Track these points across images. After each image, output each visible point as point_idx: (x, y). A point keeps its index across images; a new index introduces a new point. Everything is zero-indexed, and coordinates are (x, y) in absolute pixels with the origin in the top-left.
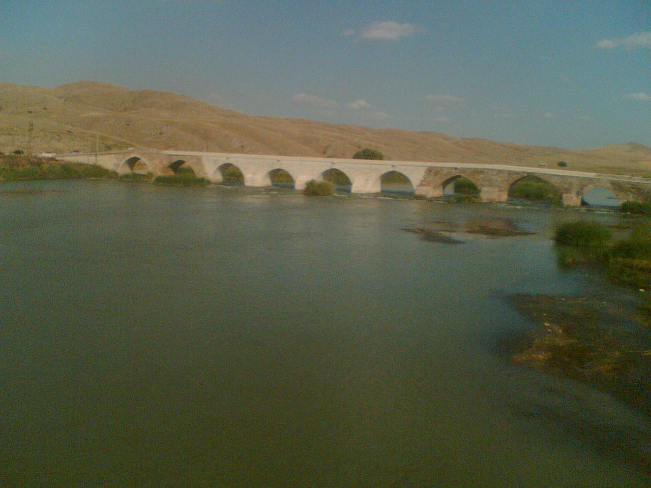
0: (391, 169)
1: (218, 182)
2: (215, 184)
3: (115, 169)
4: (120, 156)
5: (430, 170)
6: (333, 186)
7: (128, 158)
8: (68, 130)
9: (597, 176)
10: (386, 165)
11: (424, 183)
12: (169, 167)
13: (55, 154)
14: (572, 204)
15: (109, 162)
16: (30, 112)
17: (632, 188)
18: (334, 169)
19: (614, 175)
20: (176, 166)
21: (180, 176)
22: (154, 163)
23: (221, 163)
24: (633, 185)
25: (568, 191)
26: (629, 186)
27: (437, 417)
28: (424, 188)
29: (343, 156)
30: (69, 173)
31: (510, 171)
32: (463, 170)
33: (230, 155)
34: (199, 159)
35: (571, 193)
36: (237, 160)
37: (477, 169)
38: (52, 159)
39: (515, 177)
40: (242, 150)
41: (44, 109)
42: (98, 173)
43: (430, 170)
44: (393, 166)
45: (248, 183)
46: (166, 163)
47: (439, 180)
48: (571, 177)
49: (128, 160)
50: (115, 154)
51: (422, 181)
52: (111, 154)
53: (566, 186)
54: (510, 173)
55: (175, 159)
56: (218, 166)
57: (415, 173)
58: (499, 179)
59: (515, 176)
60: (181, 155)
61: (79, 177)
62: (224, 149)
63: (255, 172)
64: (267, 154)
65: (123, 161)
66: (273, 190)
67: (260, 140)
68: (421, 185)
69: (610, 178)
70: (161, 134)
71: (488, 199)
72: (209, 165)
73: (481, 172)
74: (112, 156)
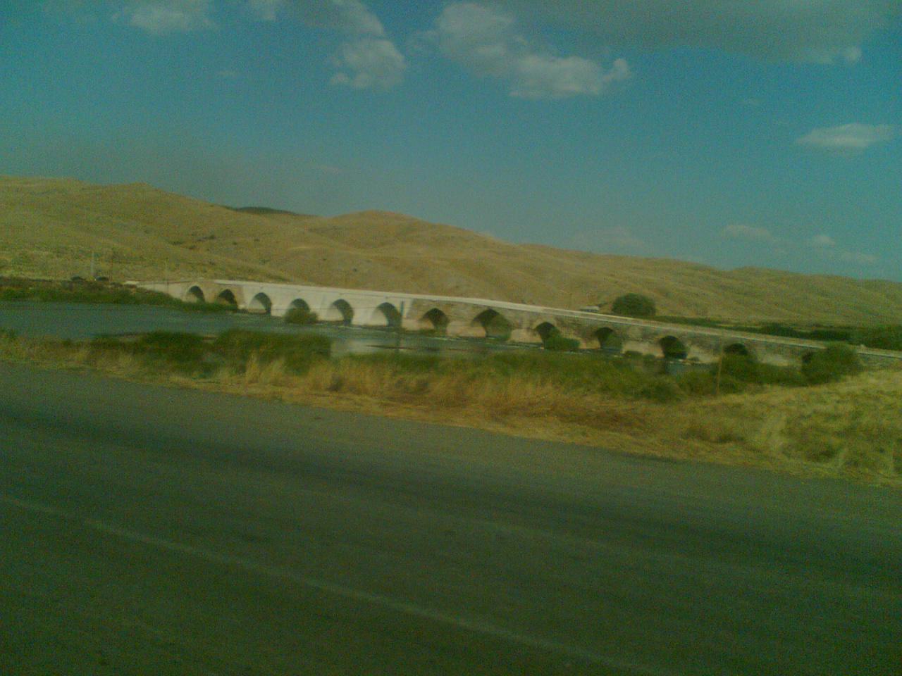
1: (257, 312)
6: (226, 303)
7: (190, 287)
10: (373, 296)
13: (138, 282)
15: (178, 291)
18: (668, 336)
22: (210, 296)
23: (257, 292)
25: (519, 327)
26: (570, 322)
27: (217, 598)
32: (439, 303)
34: (240, 288)
37: (449, 302)
39: (479, 311)
42: (161, 300)
44: (387, 298)
46: (218, 292)
47: (422, 313)
49: (663, 339)
52: (723, 327)
53: (518, 321)
54: (476, 306)
55: (224, 288)
56: (254, 295)
60: (510, 310)
61: (137, 302)
62: (383, 286)
65: (187, 291)
69: (555, 314)
73: (451, 305)
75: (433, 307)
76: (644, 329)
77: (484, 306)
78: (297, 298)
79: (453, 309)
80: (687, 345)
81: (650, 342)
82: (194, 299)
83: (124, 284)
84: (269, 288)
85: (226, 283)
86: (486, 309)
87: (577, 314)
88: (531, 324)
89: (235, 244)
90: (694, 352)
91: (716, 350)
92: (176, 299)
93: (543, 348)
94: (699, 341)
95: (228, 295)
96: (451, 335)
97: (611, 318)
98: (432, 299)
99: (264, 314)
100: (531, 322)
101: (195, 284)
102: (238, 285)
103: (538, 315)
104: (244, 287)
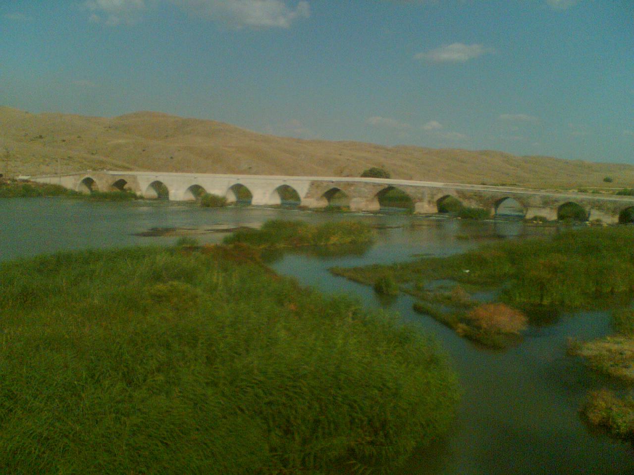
0: (283, 183)
1: (148, 197)
2: (150, 199)
3: (74, 188)
4: (77, 177)
5: (313, 184)
7: (83, 178)
8: (69, 156)
9: (444, 185)
11: (309, 195)
12: (114, 185)
14: (423, 211)
15: (70, 182)
16: (64, 141)
17: (475, 196)
19: (473, 185)
20: (121, 184)
21: (121, 192)
22: (103, 184)
24: (476, 193)
25: (421, 200)
26: (472, 194)
28: (308, 200)
29: (357, 177)
30: (28, 191)
31: (375, 183)
32: (339, 183)
33: (240, 176)
34: (135, 177)
35: (423, 202)
36: (163, 177)
38: (27, 181)
39: (380, 189)
40: (249, 171)
41: (78, 137)
42: (57, 191)
43: (313, 184)
45: (172, 197)
48: (423, 187)
50: (73, 175)
51: (307, 193)
53: (420, 196)
55: (118, 179)
57: (301, 185)
58: (366, 191)
59: (378, 187)
60: (411, 186)
61: (39, 195)
63: (179, 189)
64: (272, 174)
66: (379, 212)
67: (265, 160)
68: (307, 197)
69: (456, 187)
70: (172, 158)
71: (356, 208)
72: (142, 183)
74: (71, 177)
75: (332, 186)
76: (543, 197)
77: (385, 184)
78: (194, 183)
79: (352, 188)
80: (587, 209)
81: (551, 208)
82: (86, 190)
83: (17, 178)
84: (163, 177)
85: (120, 174)
86: (387, 186)
87: (478, 188)
88: (433, 198)
89: (64, 141)
90: (595, 215)
91: (614, 212)
92: (212, 195)
93: (460, 218)
94: (599, 206)
95: (121, 184)
96: (355, 210)
97: (512, 189)
98: (331, 179)
99: (155, 199)
100: (433, 196)
101: (87, 176)
102: (133, 176)
103: (439, 189)
104: (138, 177)
